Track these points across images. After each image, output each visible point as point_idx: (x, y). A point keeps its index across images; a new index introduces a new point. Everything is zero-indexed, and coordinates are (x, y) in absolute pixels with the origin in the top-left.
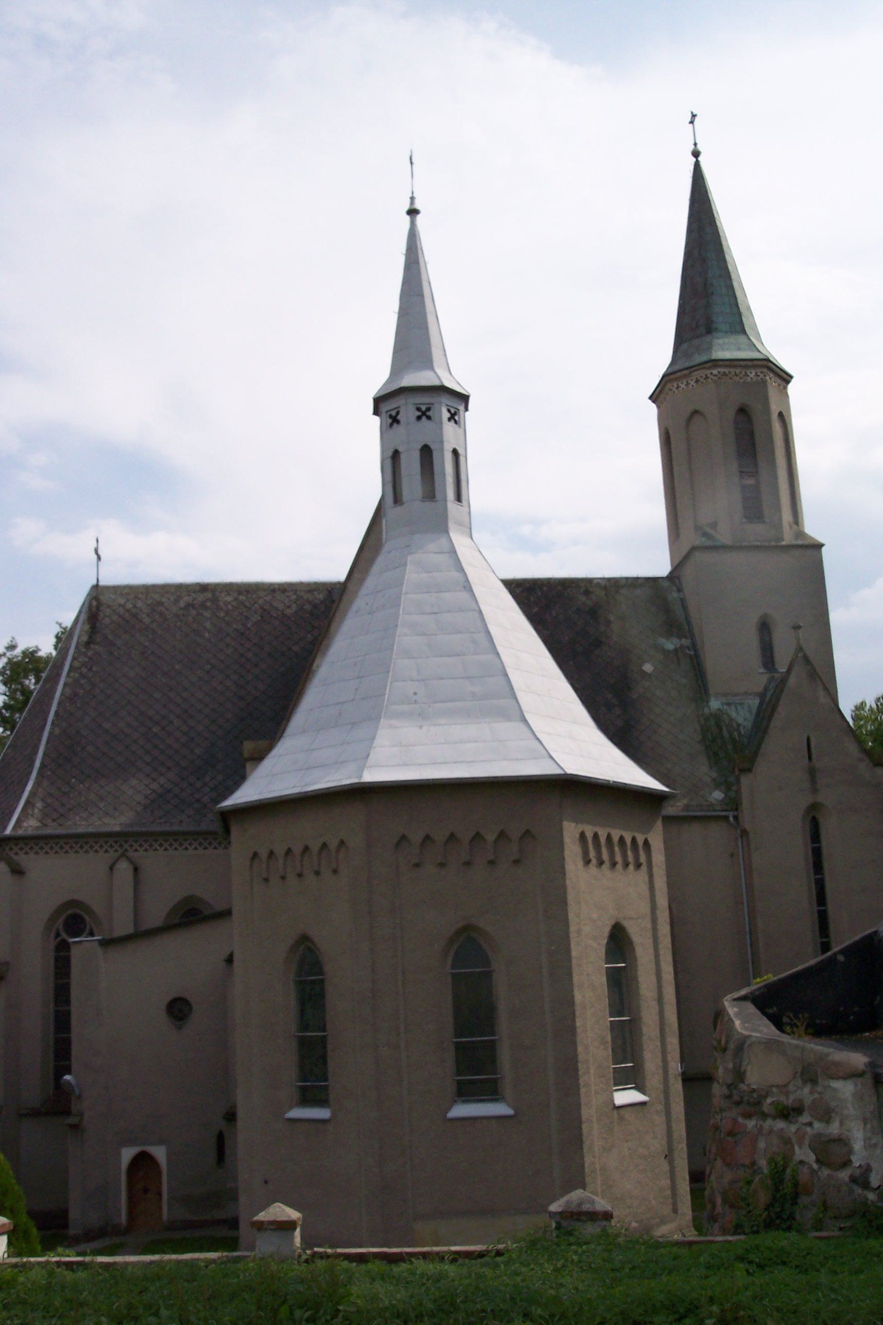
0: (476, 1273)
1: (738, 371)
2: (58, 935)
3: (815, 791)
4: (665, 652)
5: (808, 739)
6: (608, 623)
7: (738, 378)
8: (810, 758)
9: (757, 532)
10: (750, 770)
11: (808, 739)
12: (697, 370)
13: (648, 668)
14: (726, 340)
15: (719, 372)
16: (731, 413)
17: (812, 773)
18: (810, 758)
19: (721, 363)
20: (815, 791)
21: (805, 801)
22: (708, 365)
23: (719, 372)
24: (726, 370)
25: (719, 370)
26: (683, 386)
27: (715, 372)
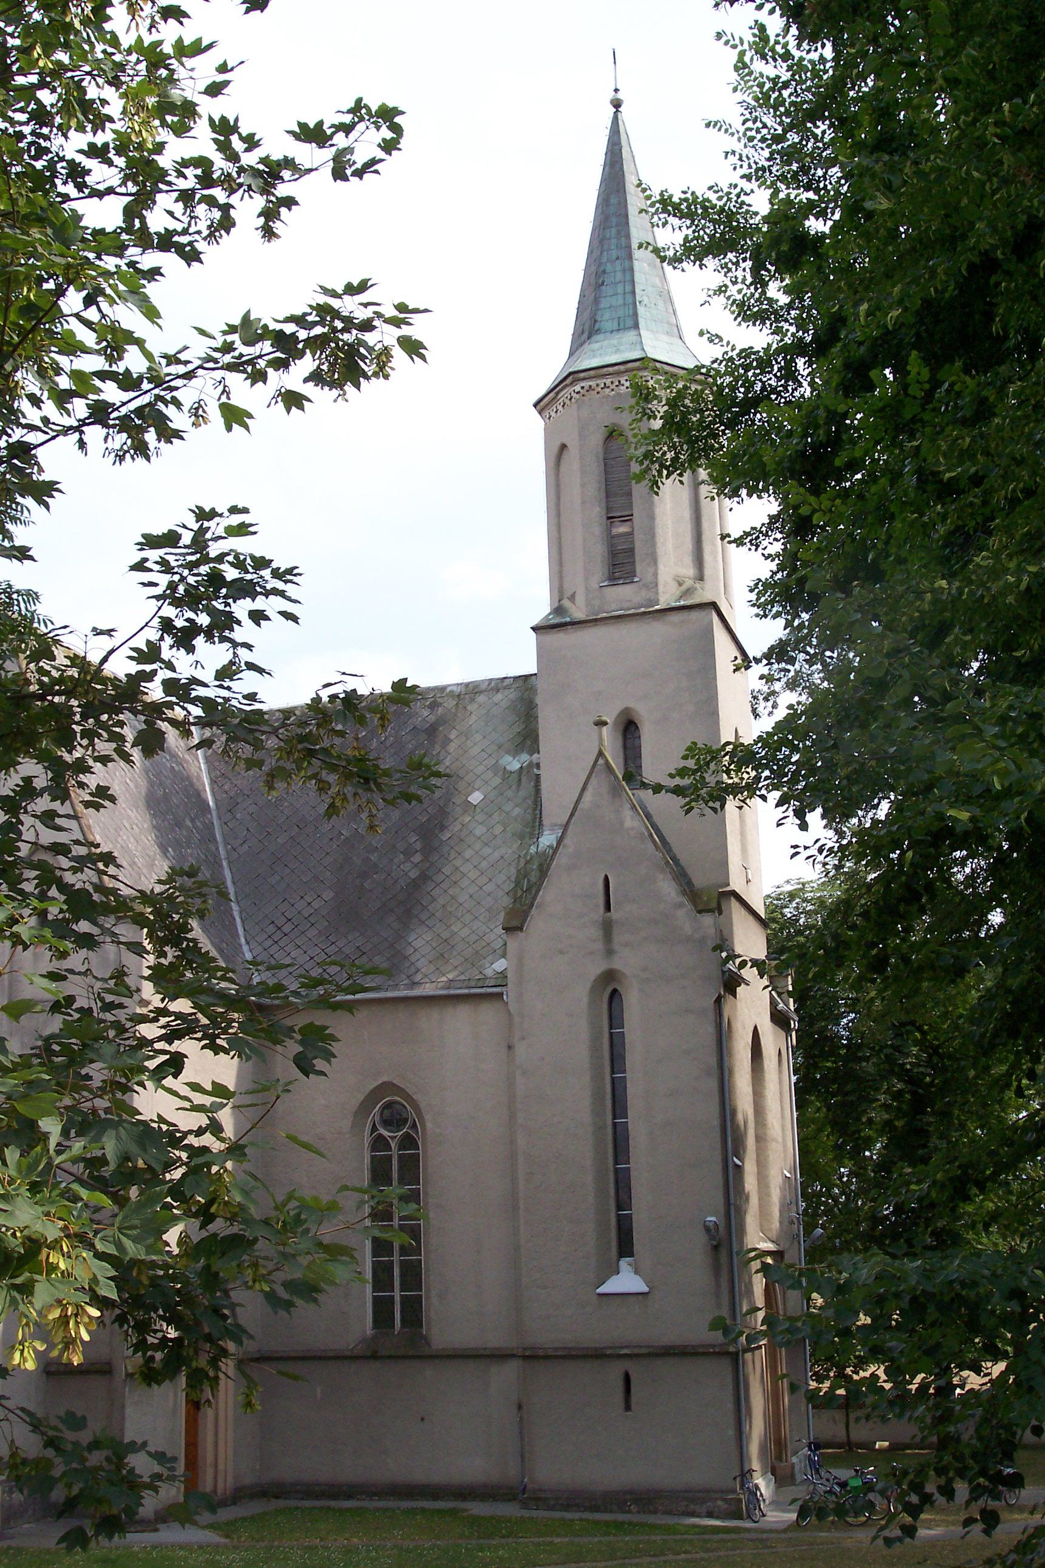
0: (991, 1520)
1: (608, 382)
2: (374, 1128)
3: (610, 952)
4: (506, 774)
5: (606, 879)
6: (447, 741)
7: (607, 391)
8: (608, 908)
9: (623, 596)
10: (521, 929)
11: (606, 879)
12: (561, 390)
13: (476, 798)
14: (606, 343)
15: (583, 388)
16: (596, 439)
17: (607, 928)
18: (608, 908)
19: (582, 375)
20: (610, 952)
21: (595, 968)
22: (568, 381)
23: (583, 388)
24: (593, 383)
25: (583, 384)
26: (553, 414)
27: (577, 388)
